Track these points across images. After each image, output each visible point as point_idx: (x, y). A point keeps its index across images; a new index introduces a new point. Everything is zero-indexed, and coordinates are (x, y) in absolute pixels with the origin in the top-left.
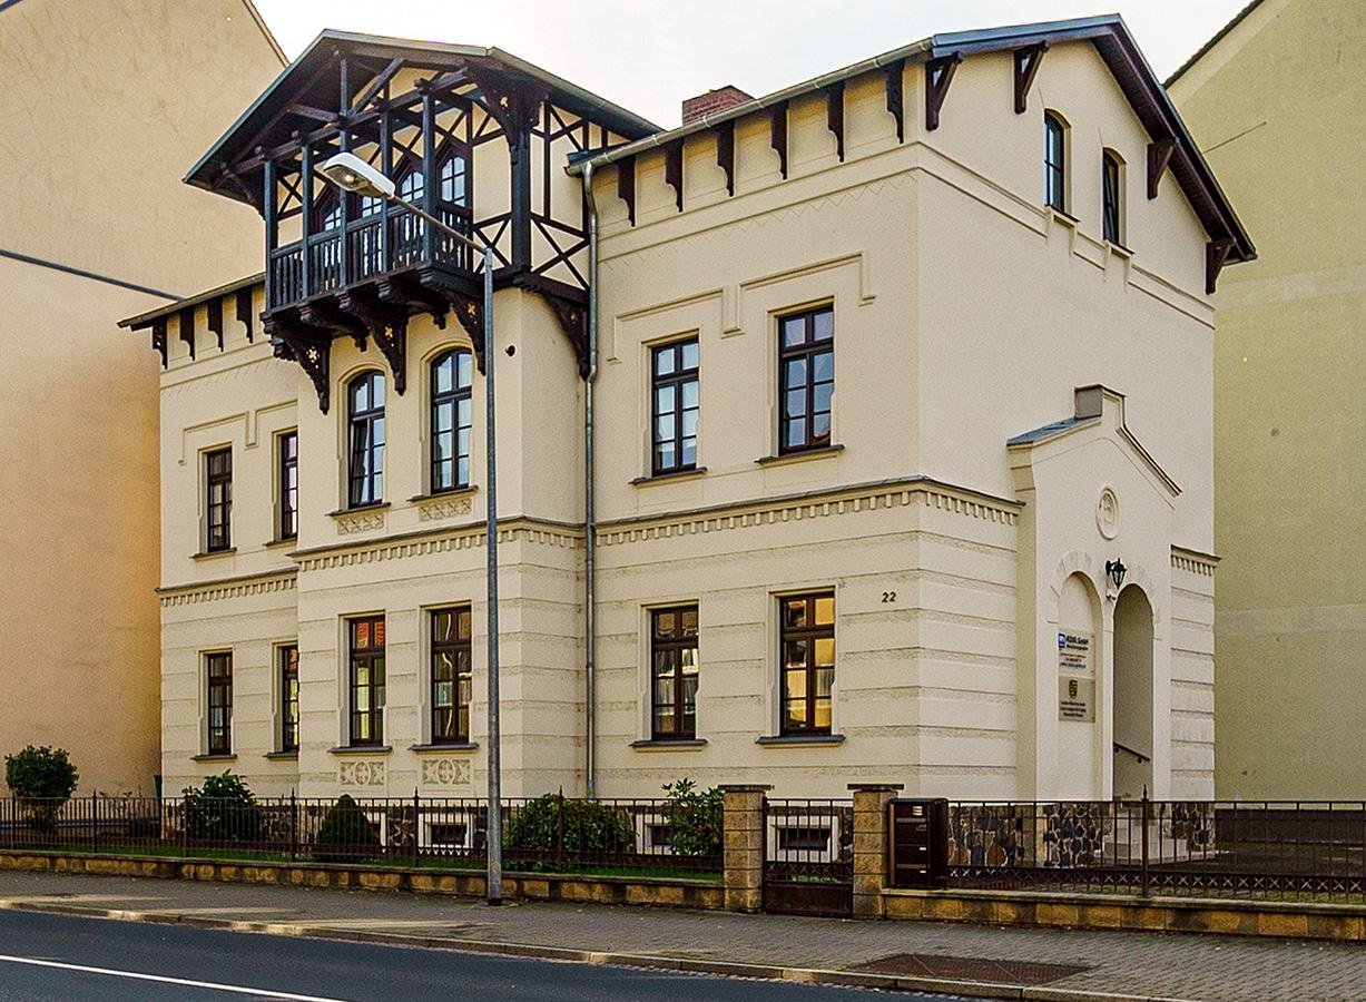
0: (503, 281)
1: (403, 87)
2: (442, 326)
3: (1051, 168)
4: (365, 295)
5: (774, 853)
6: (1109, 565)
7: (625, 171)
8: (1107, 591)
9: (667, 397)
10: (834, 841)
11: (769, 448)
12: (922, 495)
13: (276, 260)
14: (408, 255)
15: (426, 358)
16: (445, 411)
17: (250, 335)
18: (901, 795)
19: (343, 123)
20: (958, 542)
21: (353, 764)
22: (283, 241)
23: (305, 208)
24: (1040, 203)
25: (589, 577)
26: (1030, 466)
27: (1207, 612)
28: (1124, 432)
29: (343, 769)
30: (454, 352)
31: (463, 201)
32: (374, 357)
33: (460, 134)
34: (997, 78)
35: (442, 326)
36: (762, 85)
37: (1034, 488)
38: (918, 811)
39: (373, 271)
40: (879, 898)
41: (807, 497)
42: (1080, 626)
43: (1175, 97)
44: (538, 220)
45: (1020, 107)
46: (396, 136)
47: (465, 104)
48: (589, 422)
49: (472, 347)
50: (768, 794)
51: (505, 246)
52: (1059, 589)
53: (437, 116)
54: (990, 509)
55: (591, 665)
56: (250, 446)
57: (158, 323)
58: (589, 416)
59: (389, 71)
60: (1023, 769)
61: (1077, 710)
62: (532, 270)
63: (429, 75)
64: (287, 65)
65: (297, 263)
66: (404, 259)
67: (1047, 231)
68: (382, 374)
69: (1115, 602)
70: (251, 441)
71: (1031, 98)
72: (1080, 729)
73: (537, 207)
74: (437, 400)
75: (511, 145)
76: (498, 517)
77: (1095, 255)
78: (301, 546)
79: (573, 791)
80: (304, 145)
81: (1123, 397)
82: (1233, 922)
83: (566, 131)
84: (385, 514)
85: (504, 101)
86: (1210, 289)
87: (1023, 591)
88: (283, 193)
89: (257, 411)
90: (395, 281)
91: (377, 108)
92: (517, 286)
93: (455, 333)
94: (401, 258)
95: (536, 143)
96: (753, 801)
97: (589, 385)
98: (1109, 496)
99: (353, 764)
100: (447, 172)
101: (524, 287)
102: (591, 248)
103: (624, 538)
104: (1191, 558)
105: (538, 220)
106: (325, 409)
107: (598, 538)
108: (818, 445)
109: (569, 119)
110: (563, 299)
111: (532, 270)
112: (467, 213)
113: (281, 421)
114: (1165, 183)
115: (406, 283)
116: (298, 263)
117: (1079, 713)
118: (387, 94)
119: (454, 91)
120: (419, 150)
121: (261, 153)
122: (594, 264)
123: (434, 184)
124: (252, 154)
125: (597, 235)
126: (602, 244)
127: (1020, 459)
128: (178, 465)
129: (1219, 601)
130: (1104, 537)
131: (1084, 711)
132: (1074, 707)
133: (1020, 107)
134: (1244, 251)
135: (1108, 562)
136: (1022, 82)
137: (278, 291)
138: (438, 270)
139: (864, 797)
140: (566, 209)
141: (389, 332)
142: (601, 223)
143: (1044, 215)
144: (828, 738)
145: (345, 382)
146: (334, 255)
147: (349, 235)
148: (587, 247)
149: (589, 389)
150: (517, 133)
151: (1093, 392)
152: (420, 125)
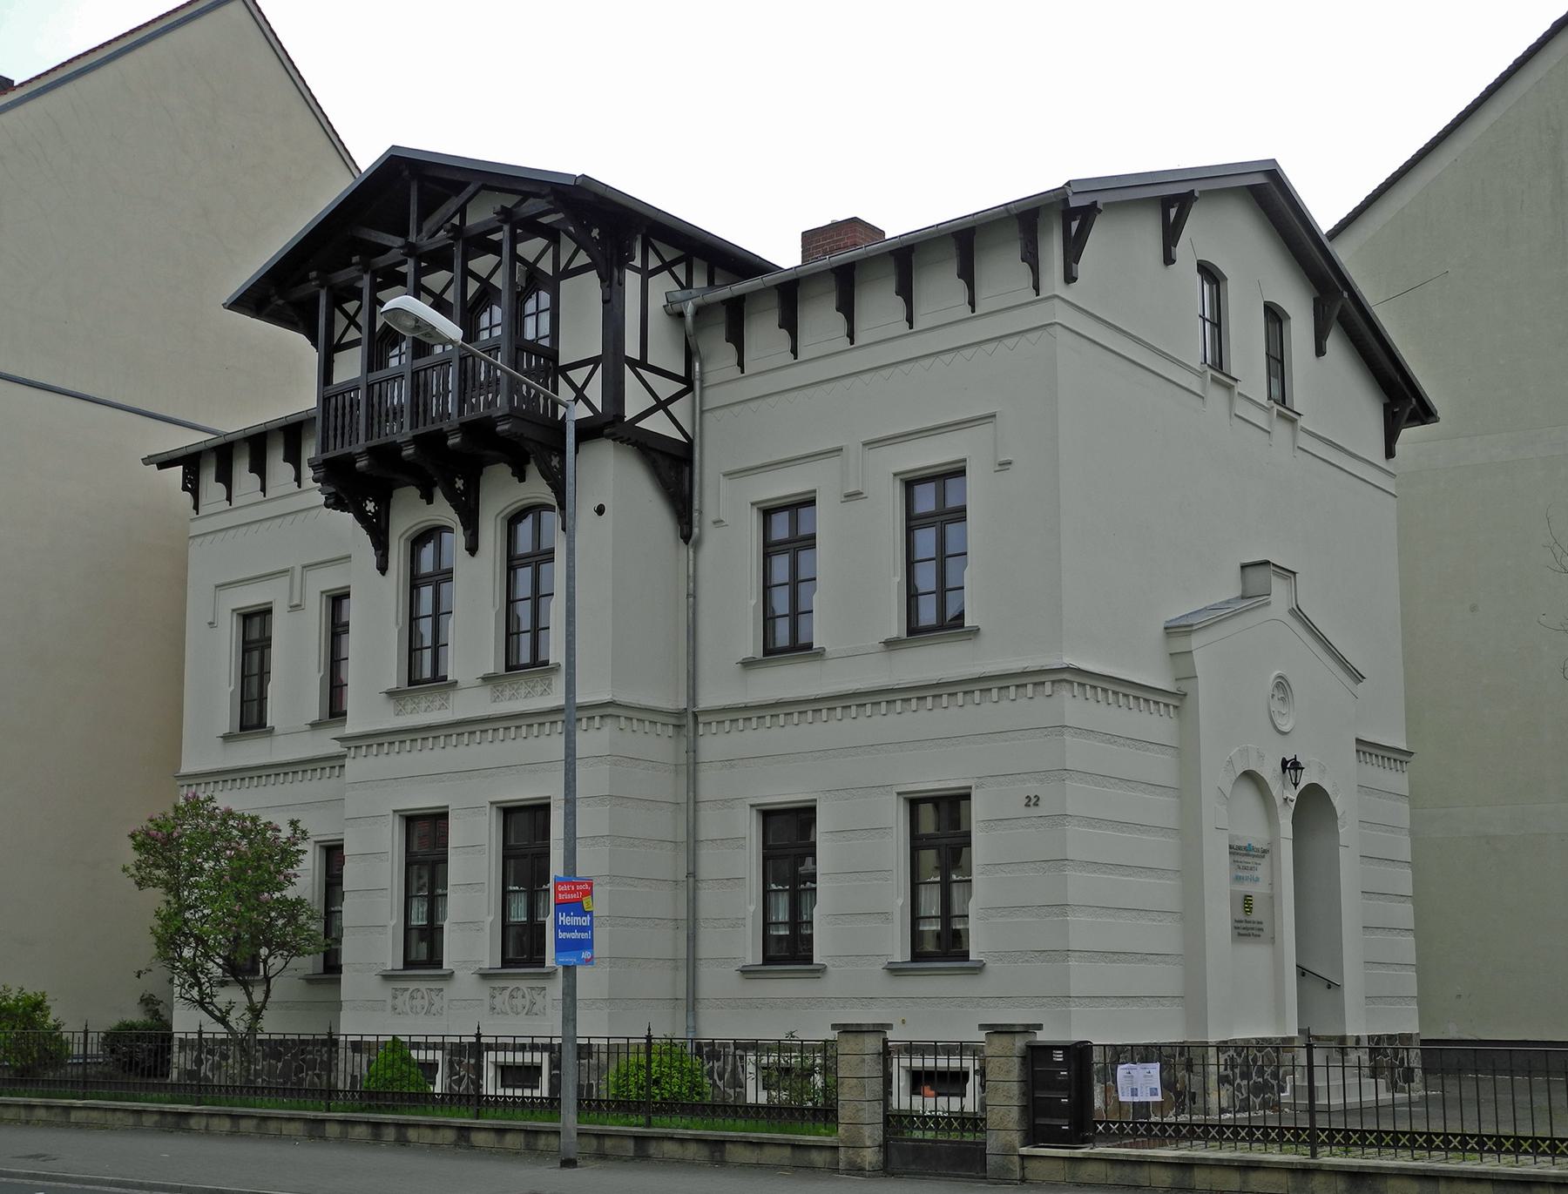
0: (589, 432)
1: (480, 214)
2: (522, 479)
3: (1207, 324)
4: (431, 443)
5: (902, 1099)
6: (1284, 762)
7: (735, 316)
8: (1284, 793)
9: (781, 565)
10: (971, 1086)
11: (896, 627)
12: (1067, 686)
13: (329, 398)
14: (482, 398)
15: (502, 515)
16: (524, 575)
17: (298, 479)
18: (1042, 1037)
19: (411, 250)
20: (1112, 738)
21: (407, 989)
22: (339, 377)
23: (365, 341)
24: (1196, 363)
25: (691, 768)
26: (1191, 652)
27: (1402, 813)
28: (1297, 613)
29: (395, 998)
30: (535, 509)
31: (548, 339)
32: (442, 512)
33: (546, 265)
34: (1149, 231)
35: (522, 479)
36: (896, 222)
37: (1196, 677)
38: (1058, 1056)
39: (444, 415)
40: (1016, 1159)
41: (938, 685)
42: (1254, 832)
43: (1343, 252)
44: (633, 364)
45: (1169, 259)
46: (473, 265)
47: (552, 234)
48: (691, 592)
49: (556, 504)
50: (890, 1035)
51: (595, 392)
52: (1228, 789)
53: (518, 246)
54: (1156, 703)
55: (692, 874)
56: (295, 608)
57: (191, 462)
58: (691, 585)
59: (465, 195)
60: (1192, 1000)
61: (1253, 929)
62: (626, 420)
63: (510, 201)
64: (357, 175)
65: (354, 404)
66: (478, 401)
67: (1204, 389)
68: (450, 530)
69: (1293, 804)
70: (296, 602)
71: (1181, 250)
72: (1255, 954)
73: (632, 350)
74: (516, 563)
75: (602, 281)
76: (577, 701)
77: (1260, 418)
78: (352, 726)
79: (668, 1026)
80: (366, 272)
81: (1294, 573)
82: (428, 1135)
83: (666, 266)
84: (451, 693)
85: (595, 233)
86: (1390, 453)
87: (1186, 791)
88: (341, 322)
89: (304, 567)
90: (468, 428)
91: (450, 235)
92: (608, 437)
93: (536, 489)
94: (474, 400)
95: (632, 281)
96: (872, 1044)
97: (691, 553)
98: (1282, 684)
99: (407, 989)
100: (530, 306)
101: (615, 438)
102: (694, 394)
103: (731, 726)
104: (1380, 753)
105: (633, 364)
106: (383, 568)
107: (701, 726)
108: (952, 625)
109: (670, 254)
110: (662, 453)
111: (626, 420)
112: (552, 354)
113: (332, 580)
114: (1333, 343)
115: (479, 431)
116: (355, 402)
117: (1255, 932)
118: (463, 220)
119: (539, 220)
120: (498, 281)
121: (315, 279)
122: (699, 413)
123: (516, 319)
124: (305, 280)
125: (702, 381)
126: (708, 392)
127: (1179, 645)
128: (208, 626)
129: (1413, 798)
130: (1275, 727)
131: (1262, 930)
132: (1248, 926)
133: (1169, 259)
134: (1424, 413)
135: (1284, 759)
136: (1171, 235)
137: (331, 433)
138: (517, 417)
139: (997, 1040)
140: (665, 354)
141: (459, 484)
142: (707, 368)
143: (1201, 374)
144: (966, 964)
145: (406, 539)
146: (399, 395)
147: (415, 374)
148: (689, 396)
149: (691, 557)
150: (610, 270)
151: (1262, 568)
152: (500, 255)
